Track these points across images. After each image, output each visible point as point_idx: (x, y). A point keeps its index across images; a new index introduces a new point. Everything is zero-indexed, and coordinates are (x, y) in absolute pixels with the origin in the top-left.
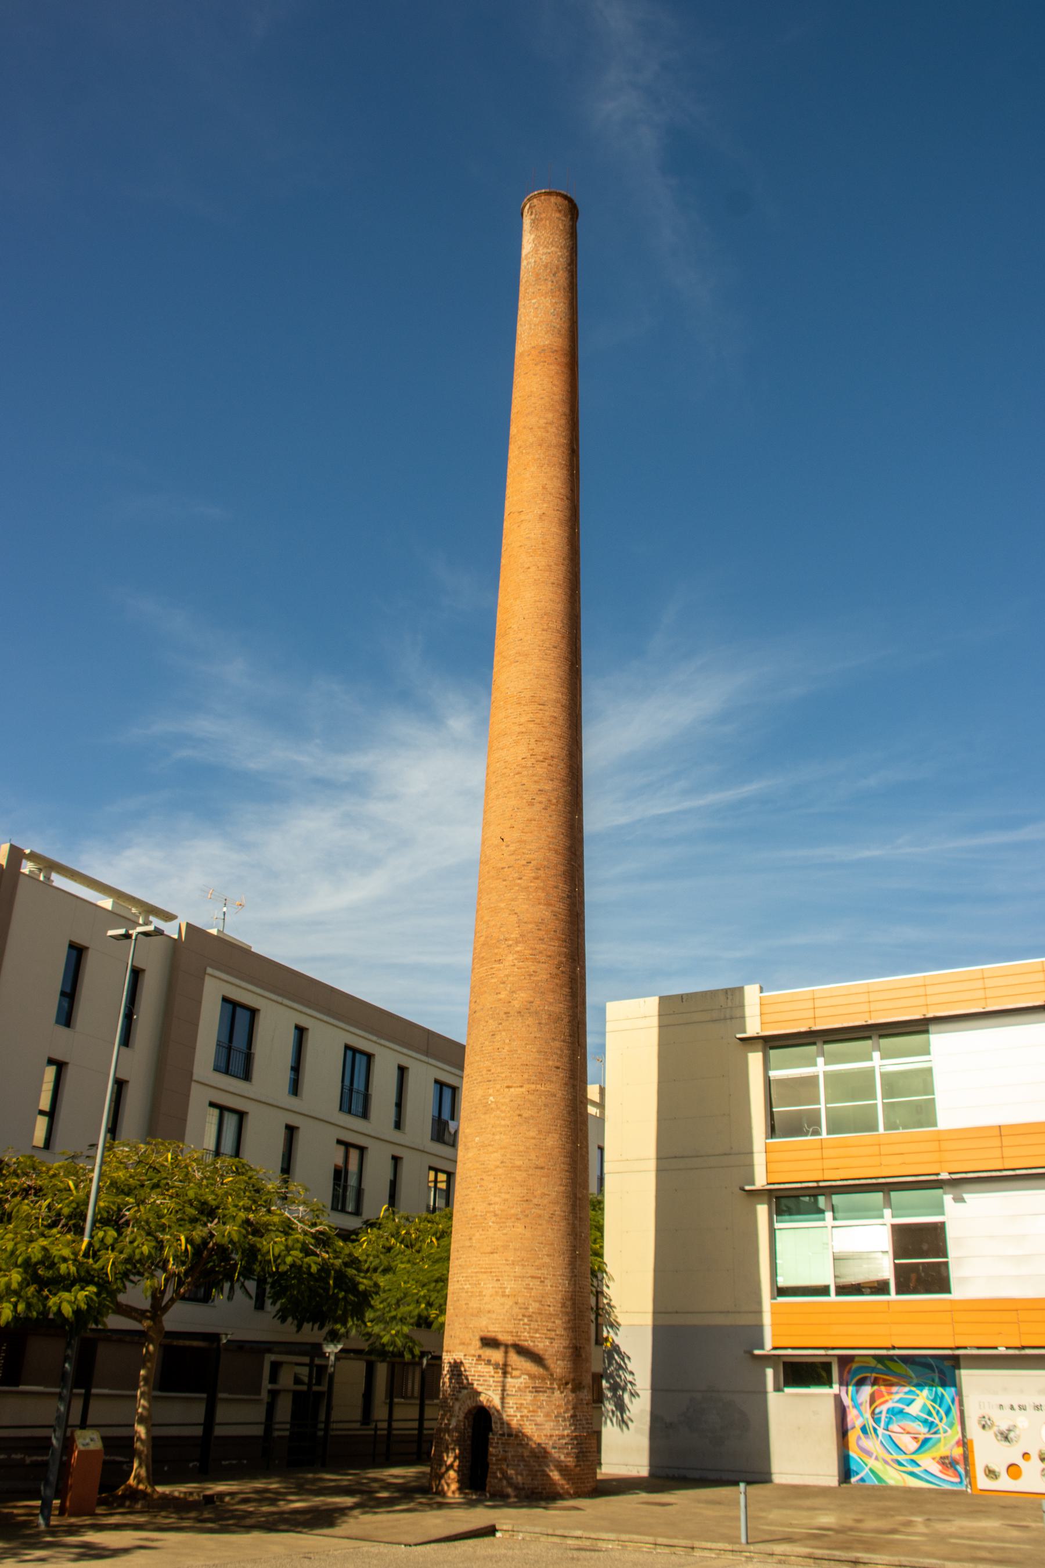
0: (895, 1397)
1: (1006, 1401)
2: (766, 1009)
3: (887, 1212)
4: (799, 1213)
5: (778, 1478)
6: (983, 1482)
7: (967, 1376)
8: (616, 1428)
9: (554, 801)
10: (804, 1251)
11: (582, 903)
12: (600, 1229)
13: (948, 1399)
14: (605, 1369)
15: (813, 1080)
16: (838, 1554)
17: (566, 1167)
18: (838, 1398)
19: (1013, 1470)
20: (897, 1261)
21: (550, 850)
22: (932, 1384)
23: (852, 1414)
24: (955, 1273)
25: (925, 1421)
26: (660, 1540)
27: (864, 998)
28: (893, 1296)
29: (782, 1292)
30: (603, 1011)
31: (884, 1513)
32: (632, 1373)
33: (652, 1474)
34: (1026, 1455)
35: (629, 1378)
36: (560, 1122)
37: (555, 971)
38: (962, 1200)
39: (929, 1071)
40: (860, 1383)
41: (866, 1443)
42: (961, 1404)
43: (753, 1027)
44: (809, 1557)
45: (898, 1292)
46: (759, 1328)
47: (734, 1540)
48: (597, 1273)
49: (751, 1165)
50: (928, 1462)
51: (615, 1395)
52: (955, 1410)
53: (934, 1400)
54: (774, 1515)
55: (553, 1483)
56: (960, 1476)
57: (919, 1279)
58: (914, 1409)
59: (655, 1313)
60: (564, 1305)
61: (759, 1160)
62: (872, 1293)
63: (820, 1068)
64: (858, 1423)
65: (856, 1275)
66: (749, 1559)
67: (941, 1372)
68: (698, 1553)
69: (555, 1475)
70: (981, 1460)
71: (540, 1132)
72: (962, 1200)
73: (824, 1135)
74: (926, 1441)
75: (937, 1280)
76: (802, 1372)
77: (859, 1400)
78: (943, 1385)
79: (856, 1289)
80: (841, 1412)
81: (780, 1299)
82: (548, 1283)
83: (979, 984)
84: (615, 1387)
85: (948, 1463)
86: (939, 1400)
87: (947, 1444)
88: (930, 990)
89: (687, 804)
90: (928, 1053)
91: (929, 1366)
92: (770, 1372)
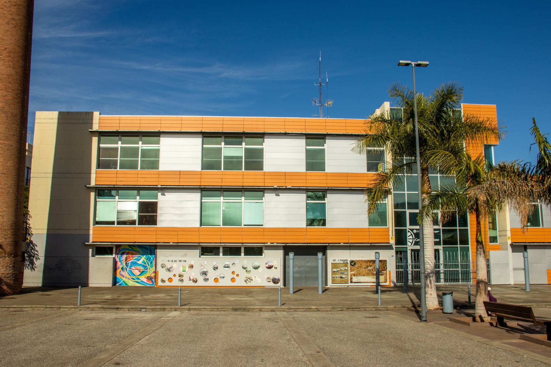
0: (133, 258)
1: (170, 259)
2: (102, 121)
3: (138, 197)
4: (104, 196)
5: (90, 285)
6: (160, 284)
7: (159, 252)
8: (30, 270)
9: (19, 25)
10: (106, 209)
11: (29, 70)
12: (27, 198)
13: (152, 259)
14: (26, 250)
15: (116, 149)
16: (111, 306)
17: (15, 174)
18: (114, 259)
19: (170, 280)
20: (307, 147)
21: (16, 45)
22: (147, 254)
23: (119, 264)
24: (159, 219)
25: (144, 266)
26: (48, 306)
27: (139, 122)
28: (116, 225)
29: (97, 223)
30: (35, 114)
31: (127, 294)
32: (37, 251)
33: (43, 286)
34: (175, 275)
35: (36, 253)
36: (13, 157)
37: (15, 96)
38: (164, 195)
39: (159, 150)
40: (123, 254)
41: (122, 273)
42: (156, 260)
43: (96, 127)
44: (102, 308)
45: (139, 224)
46: (88, 235)
47: (76, 304)
48: (26, 214)
49: (90, 178)
50: (143, 278)
51: (30, 259)
52: (154, 263)
53: (147, 259)
54: (89, 296)
55: (4, 290)
56: (153, 282)
57: (146, 221)
58: (140, 262)
59: (48, 229)
60: (11, 226)
61: (93, 176)
62: (130, 224)
63: (120, 145)
64: (121, 267)
65: (124, 218)
66: (80, 310)
67: (151, 251)
68: (62, 309)
69: (5, 287)
70: (160, 278)
71: (5, 160)
72: (164, 195)
73: (118, 169)
74: (143, 272)
75: (153, 221)
76: (102, 250)
77: (122, 260)
78: (151, 254)
79: (124, 223)
80: (115, 263)
81: (96, 225)
82: (5, 218)
83: (180, 122)
84: (30, 256)
85: (149, 278)
86: (149, 259)
87: (150, 273)
88: (162, 122)
89: (74, 35)
90: (159, 144)
91: (147, 248)
92: (91, 250)
